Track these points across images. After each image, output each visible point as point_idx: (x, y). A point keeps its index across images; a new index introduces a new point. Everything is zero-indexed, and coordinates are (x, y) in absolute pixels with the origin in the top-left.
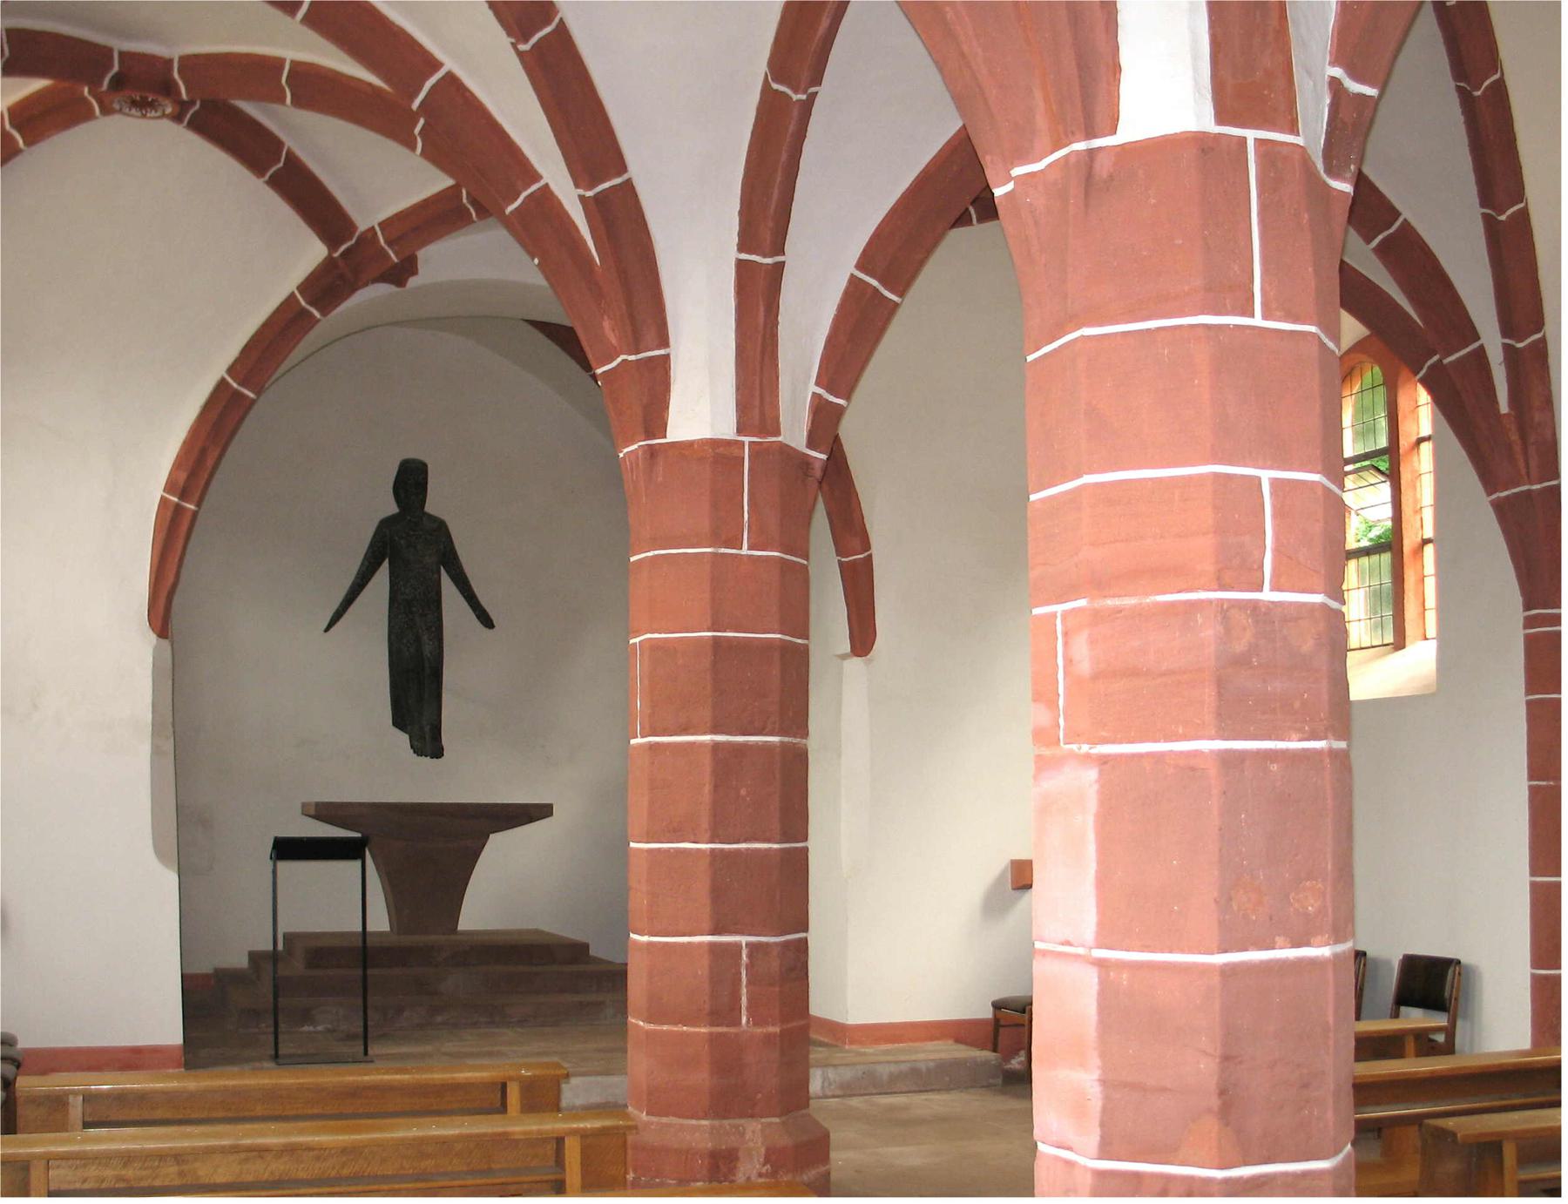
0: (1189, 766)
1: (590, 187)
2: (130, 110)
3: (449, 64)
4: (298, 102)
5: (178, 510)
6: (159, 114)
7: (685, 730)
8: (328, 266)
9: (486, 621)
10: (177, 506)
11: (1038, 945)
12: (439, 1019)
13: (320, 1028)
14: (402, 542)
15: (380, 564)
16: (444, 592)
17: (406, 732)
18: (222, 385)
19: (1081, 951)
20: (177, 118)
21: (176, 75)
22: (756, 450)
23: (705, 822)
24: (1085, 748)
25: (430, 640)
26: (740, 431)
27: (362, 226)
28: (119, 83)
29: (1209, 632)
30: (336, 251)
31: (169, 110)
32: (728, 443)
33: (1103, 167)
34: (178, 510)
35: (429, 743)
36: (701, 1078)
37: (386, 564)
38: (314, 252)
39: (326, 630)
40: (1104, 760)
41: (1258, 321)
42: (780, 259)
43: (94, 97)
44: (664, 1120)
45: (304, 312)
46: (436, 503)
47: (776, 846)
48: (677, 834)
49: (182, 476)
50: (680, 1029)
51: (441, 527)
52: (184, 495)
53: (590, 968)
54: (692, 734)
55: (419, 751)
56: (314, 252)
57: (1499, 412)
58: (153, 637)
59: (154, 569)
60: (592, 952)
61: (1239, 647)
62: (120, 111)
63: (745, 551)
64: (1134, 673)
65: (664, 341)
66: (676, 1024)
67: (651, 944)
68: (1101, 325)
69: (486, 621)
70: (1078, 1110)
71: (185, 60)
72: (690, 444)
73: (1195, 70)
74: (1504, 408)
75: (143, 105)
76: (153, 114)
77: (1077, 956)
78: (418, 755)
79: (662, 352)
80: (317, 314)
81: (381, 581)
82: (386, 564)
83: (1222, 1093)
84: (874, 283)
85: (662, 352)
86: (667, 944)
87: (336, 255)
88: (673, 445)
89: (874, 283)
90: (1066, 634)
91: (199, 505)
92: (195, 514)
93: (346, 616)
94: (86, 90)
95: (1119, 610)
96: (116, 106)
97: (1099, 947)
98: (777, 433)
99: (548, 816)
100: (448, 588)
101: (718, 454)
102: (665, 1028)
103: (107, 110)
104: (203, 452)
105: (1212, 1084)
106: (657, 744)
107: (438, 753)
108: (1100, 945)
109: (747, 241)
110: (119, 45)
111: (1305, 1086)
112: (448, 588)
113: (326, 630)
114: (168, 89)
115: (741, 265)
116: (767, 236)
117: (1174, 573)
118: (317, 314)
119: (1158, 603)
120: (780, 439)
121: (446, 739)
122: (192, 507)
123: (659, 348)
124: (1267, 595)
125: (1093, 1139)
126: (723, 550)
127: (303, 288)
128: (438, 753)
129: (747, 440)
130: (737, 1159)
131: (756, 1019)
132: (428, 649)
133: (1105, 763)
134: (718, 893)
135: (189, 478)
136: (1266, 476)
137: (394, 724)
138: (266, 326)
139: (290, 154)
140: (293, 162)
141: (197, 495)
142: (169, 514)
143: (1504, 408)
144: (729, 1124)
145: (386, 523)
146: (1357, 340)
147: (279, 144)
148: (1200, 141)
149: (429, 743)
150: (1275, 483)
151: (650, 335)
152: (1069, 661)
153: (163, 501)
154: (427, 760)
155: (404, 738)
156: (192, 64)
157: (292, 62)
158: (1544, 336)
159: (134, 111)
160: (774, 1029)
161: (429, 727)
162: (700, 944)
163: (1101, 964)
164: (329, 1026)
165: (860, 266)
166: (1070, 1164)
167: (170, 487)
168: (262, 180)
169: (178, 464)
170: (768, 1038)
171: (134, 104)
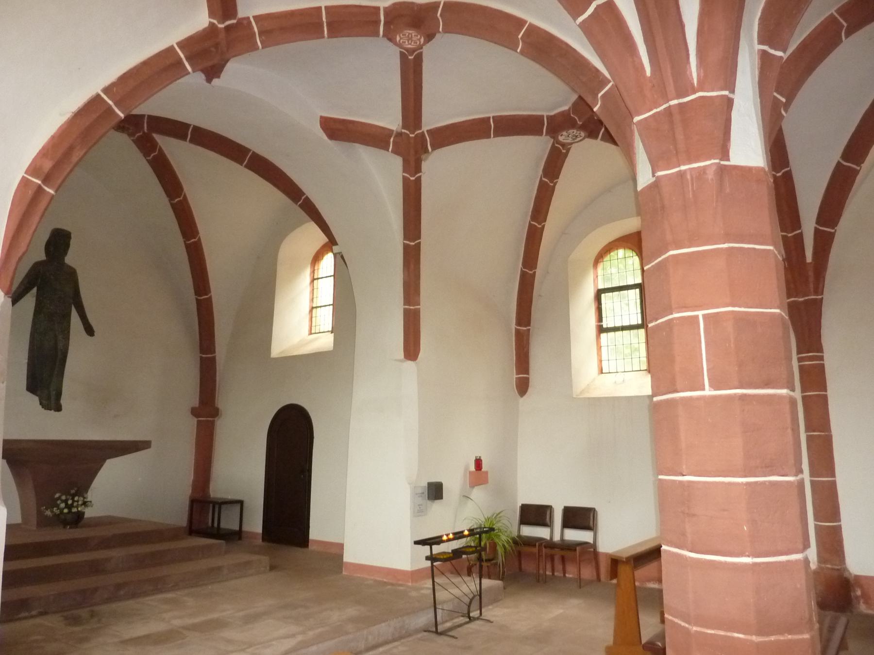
5: (39, 190)
7: (767, 385)
8: (210, 32)
10: (39, 188)
12: (122, 593)
13: (34, 613)
14: (52, 277)
15: (31, 288)
17: (37, 396)
18: (95, 101)
25: (64, 339)
34: (39, 190)
37: (35, 290)
45: (180, 62)
49: (48, 165)
50: (786, 638)
51: (72, 275)
52: (47, 179)
54: (773, 388)
57: (806, 261)
66: (781, 633)
67: (755, 564)
74: (809, 257)
78: (45, 409)
91: (56, 191)
99: (147, 448)
102: (773, 638)
104: (71, 149)
107: (58, 408)
121: (63, 402)
122: (52, 192)
128: (58, 408)
132: (60, 345)
141: (57, 186)
142: (30, 193)
143: (809, 257)
144: (347, 633)
145: (37, 265)
146: (622, 235)
153: (24, 182)
155: (36, 399)
158: (802, 231)
161: (54, 393)
164: (41, 610)
167: (33, 169)
169: (44, 153)
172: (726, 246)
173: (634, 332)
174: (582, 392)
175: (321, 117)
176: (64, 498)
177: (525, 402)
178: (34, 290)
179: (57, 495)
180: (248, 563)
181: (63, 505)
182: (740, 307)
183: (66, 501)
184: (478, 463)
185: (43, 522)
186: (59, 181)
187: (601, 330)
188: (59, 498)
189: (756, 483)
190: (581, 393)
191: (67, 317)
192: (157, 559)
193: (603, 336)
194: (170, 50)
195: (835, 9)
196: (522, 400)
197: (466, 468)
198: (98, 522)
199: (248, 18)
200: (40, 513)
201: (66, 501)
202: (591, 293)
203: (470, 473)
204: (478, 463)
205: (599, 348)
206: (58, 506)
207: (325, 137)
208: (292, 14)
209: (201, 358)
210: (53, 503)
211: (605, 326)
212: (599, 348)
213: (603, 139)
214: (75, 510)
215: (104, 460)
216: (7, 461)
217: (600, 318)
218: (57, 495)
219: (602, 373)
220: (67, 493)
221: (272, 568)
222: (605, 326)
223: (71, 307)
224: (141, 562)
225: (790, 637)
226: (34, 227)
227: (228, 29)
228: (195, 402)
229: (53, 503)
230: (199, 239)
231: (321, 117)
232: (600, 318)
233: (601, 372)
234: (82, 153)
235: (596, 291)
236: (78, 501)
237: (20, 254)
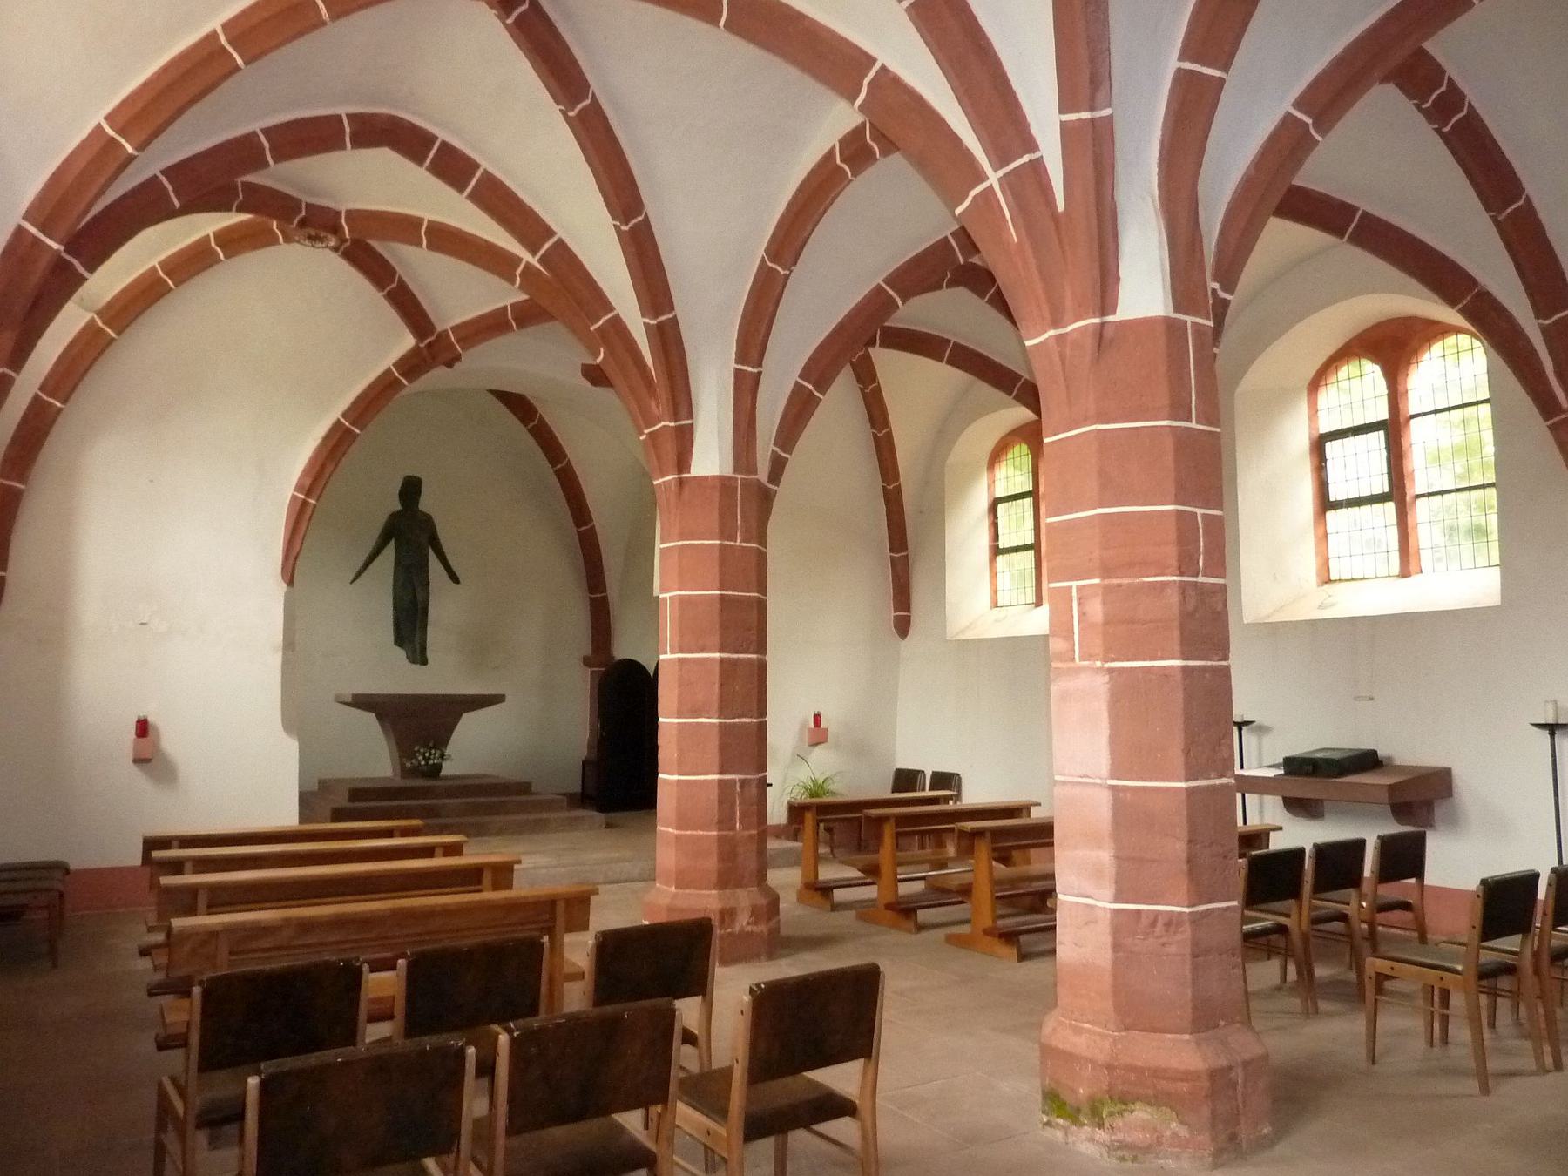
0: (1165, 673)
1: (656, 317)
2: (305, 240)
3: (561, 233)
4: (431, 247)
6: (324, 245)
7: (702, 650)
8: (415, 352)
9: (455, 579)
11: (1057, 778)
15: (389, 542)
16: (430, 559)
18: (338, 424)
19: (1098, 781)
20: (336, 249)
21: (343, 222)
22: (745, 483)
23: (715, 705)
24: (1099, 664)
26: (736, 471)
27: (439, 328)
28: (303, 224)
29: (1173, 598)
30: (422, 342)
31: (332, 244)
32: (730, 478)
33: (1109, 333)
35: (419, 656)
36: (711, 863)
37: (393, 542)
38: (408, 341)
39: (352, 582)
40: (1111, 671)
41: (1194, 425)
42: (760, 369)
43: (282, 231)
44: (687, 891)
45: (396, 379)
46: (426, 504)
47: (755, 720)
48: (696, 713)
49: (308, 483)
51: (428, 520)
52: (308, 493)
53: (533, 798)
55: (413, 661)
56: (408, 341)
58: (285, 585)
59: (286, 542)
60: (533, 789)
61: (1190, 607)
62: (298, 242)
63: (738, 543)
64: (1132, 621)
65: (690, 415)
66: (696, 830)
68: (1108, 423)
69: (455, 579)
70: (1097, 873)
71: (350, 213)
72: (706, 478)
73: (1163, 280)
75: (314, 239)
76: (320, 245)
77: (1095, 784)
79: (689, 422)
80: (405, 382)
81: (389, 553)
82: (393, 542)
83: (1189, 861)
84: (810, 387)
85: (689, 422)
86: (1163, 780)
87: (422, 345)
88: (695, 477)
89: (810, 387)
90: (1080, 599)
91: (317, 500)
92: (315, 506)
93: (364, 575)
94: (275, 224)
95: (1119, 586)
96: (297, 238)
97: (1112, 778)
98: (756, 473)
100: (433, 558)
101: (724, 484)
102: (689, 832)
103: (288, 239)
104: (323, 467)
105: (1184, 855)
106: (684, 659)
107: (424, 662)
108: (1112, 778)
109: (742, 357)
110: (306, 199)
111: (1225, 857)
112: (433, 558)
113: (352, 582)
114: (336, 230)
115: (738, 373)
116: (754, 354)
117: (1146, 566)
118: (405, 382)
119: (1144, 582)
120: (756, 477)
121: (429, 654)
123: (688, 419)
124: (1201, 579)
125: (1109, 891)
126: (726, 542)
127: (397, 365)
128: (424, 662)
129: (739, 476)
130: (736, 913)
131: (745, 828)
132: (420, 598)
133: (1112, 672)
134: (723, 748)
135: (311, 485)
136: (1200, 511)
137: (395, 644)
138: (371, 387)
139: (400, 279)
140: (403, 286)
145: (394, 516)
147: (394, 271)
148: (1166, 320)
149: (419, 656)
150: (1204, 515)
151: (684, 411)
152: (1082, 614)
153: (294, 498)
154: (417, 667)
156: (353, 215)
157: (429, 221)
159: (307, 242)
160: (754, 832)
162: (712, 781)
163: (1113, 788)
165: (801, 376)
166: (1091, 907)
167: (299, 488)
168: (382, 294)
169: (305, 473)
170: (751, 836)
171: (310, 238)
172: (680, 543)
173: (1378, 507)
174: (962, 631)
175: (583, 365)
176: (422, 750)
177: (907, 646)
178: (392, 542)
179: (416, 749)
180: (576, 819)
181: (421, 758)
182: (685, 591)
183: (424, 754)
184: (817, 719)
185: (406, 773)
186: (318, 492)
187: (1325, 504)
188: (419, 751)
189: (685, 723)
190: (957, 634)
191: (423, 567)
192: (492, 810)
193: (1000, 559)
194: (388, 372)
195: (882, 278)
196: (903, 643)
197: (803, 725)
198: (447, 778)
199: (446, 331)
200: (403, 766)
201: (424, 754)
202: (980, 502)
203: (809, 729)
204: (817, 719)
205: (994, 575)
206: (416, 758)
207: (588, 384)
208: (482, 318)
209: (591, 599)
210: (412, 756)
211: (1001, 547)
212: (994, 575)
213: (990, 302)
214: (431, 762)
215: (461, 715)
216: (376, 716)
217: (995, 536)
218: (416, 749)
219: (1329, 581)
220: (426, 746)
221: (609, 826)
222: (1001, 547)
223: (427, 556)
224: (475, 810)
225: (702, 833)
226: (303, 532)
227: (430, 345)
228: (587, 650)
229: (412, 756)
230: (569, 463)
231: (583, 365)
232: (995, 536)
233: (995, 604)
234: (332, 469)
235: (991, 502)
236: (435, 754)
237: (295, 554)
